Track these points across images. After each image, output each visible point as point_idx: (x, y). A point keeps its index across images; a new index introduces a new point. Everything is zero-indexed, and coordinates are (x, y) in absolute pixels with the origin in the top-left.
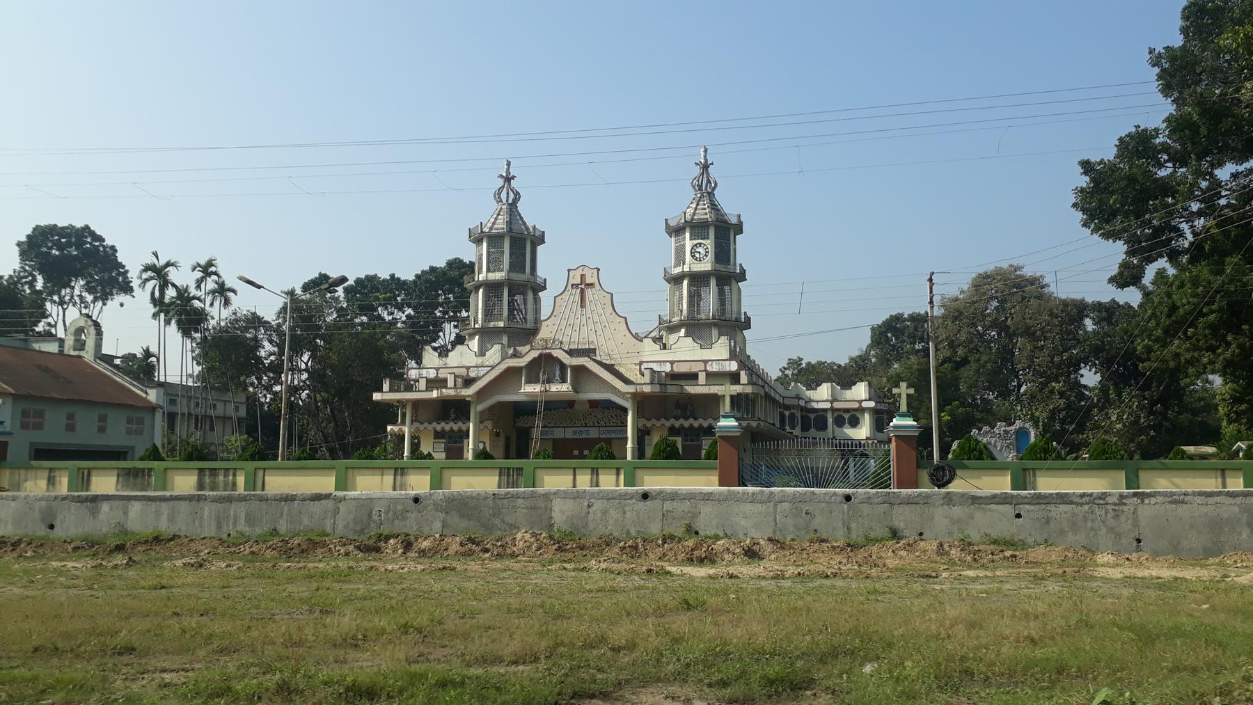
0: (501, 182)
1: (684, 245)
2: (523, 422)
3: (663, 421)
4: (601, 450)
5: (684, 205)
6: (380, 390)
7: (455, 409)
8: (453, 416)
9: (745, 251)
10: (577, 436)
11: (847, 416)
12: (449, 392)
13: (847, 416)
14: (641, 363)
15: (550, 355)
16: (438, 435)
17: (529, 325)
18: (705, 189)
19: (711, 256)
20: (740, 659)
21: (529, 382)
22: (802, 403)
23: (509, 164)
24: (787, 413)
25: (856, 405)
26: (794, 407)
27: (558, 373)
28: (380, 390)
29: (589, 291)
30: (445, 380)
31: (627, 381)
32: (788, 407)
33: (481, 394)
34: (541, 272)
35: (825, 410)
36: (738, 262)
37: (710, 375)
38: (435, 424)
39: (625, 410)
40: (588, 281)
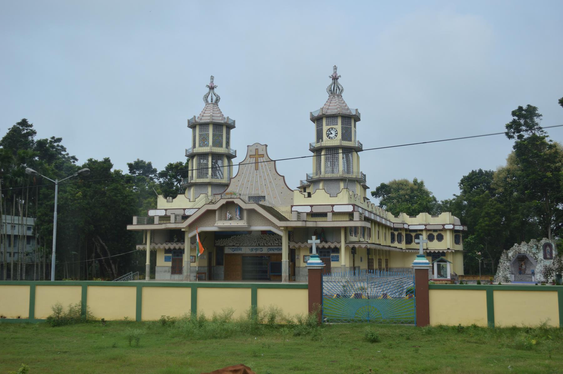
1: (322, 130)
2: (220, 243)
4: (356, 233)
6: (131, 223)
7: (176, 235)
8: (176, 239)
9: (362, 133)
10: (254, 252)
11: (435, 234)
12: (171, 225)
13: (435, 234)
14: (292, 206)
15: (233, 203)
16: (167, 251)
17: (225, 181)
18: (335, 90)
19: (340, 136)
21: (220, 219)
22: (406, 226)
23: (212, 78)
24: (396, 233)
25: (441, 227)
26: (401, 229)
27: (238, 213)
28: (131, 223)
30: (169, 217)
31: (281, 218)
32: (396, 229)
33: (192, 226)
34: (233, 146)
35: (422, 230)
36: (357, 140)
37: (334, 214)
38: (164, 245)
39: (280, 238)
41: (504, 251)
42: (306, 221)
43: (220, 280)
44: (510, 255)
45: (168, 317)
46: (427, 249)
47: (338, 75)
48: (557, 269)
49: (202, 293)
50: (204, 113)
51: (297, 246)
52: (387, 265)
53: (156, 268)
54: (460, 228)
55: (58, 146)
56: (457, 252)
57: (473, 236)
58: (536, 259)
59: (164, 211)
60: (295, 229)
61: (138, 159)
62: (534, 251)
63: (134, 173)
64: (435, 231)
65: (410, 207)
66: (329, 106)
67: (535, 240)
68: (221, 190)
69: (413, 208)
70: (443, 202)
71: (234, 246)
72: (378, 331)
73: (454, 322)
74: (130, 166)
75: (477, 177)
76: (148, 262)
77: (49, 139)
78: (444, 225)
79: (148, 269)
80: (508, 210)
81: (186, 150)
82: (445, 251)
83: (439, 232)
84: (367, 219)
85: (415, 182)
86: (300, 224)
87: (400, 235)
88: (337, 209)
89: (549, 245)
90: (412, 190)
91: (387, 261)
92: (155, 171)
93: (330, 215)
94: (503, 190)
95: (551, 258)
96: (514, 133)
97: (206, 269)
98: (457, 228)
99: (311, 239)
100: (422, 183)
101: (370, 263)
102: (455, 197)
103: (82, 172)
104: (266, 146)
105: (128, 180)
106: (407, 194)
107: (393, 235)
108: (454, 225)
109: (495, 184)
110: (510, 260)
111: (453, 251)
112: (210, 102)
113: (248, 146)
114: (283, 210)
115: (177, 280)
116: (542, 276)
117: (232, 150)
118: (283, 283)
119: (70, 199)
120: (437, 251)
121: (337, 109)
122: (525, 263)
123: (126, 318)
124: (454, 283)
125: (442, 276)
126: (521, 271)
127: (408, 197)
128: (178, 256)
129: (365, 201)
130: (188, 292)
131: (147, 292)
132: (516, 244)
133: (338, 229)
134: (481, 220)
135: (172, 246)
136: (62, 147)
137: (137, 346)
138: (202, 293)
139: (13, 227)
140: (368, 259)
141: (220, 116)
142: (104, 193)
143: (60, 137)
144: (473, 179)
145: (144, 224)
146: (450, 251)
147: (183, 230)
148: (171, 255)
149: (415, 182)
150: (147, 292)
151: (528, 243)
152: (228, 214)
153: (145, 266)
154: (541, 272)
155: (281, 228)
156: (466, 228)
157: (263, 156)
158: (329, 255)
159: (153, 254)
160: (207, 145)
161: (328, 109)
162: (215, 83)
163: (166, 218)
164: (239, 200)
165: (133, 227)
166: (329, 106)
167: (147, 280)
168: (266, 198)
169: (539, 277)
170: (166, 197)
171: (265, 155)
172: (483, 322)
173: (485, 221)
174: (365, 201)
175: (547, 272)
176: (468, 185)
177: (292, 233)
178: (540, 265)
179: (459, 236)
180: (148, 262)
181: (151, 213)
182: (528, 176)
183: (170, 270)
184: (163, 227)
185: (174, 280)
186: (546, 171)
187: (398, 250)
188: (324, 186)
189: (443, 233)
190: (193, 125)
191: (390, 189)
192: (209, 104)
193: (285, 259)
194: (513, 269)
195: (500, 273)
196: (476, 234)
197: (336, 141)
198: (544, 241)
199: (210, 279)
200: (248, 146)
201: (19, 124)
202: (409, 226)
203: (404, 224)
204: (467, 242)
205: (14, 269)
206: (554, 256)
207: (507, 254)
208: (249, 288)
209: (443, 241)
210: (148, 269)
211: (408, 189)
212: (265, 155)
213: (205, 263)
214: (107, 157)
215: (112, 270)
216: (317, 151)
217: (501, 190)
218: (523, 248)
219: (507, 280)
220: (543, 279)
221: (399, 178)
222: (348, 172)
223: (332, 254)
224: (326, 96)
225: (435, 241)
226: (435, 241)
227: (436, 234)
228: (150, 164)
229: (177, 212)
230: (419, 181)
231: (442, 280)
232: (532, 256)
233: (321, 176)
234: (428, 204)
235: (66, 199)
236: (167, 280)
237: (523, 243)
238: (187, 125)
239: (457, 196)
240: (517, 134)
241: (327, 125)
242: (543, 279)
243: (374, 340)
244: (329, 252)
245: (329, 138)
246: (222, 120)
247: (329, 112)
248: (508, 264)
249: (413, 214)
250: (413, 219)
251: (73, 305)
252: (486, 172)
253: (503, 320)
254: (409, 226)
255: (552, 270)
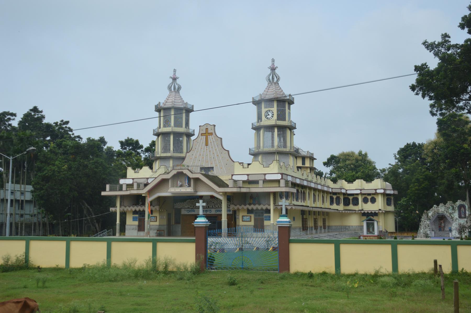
0: (171, 80)
1: (261, 111)
2: (178, 206)
3: (243, 206)
5: (260, 88)
6: (105, 190)
7: (139, 200)
8: (141, 203)
9: (295, 114)
12: (135, 192)
13: (369, 197)
14: (232, 175)
15: (182, 173)
16: (135, 212)
17: (183, 155)
18: (273, 78)
19: (275, 117)
20: (413, 279)
21: (173, 186)
22: (343, 191)
23: (175, 71)
24: (335, 197)
25: (374, 192)
26: (339, 193)
27: (187, 182)
28: (105, 190)
29: (210, 138)
32: (335, 194)
33: (151, 192)
35: (358, 194)
37: (265, 181)
38: (131, 207)
39: (220, 201)
40: (209, 132)
41: (425, 211)
42: (240, 187)
43: (178, 236)
44: (430, 214)
45: (88, 265)
46: (362, 210)
47: (275, 66)
48: (469, 227)
49: (160, 246)
50: (168, 100)
51: (236, 208)
52: (324, 223)
53: (126, 227)
54: (392, 192)
55: (66, 127)
56: (387, 213)
57: (406, 199)
58: (452, 218)
59: (131, 180)
60: (234, 194)
61: (128, 138)
62: (450, 211)
63: (125, 149)
64: (369, 194)
65: (354, 175)
66: (267, 92)
67: (451, 202)
68: (178, 162)
69: (357, 175)
70: (381, 170)
71: (188, 208)
72: (237, 276)
73: (307, 270)
74: (121, 143)
75: (411, 149)
76: (118, 222)
77: (59, 122)
78: (376, 190)
79: (118, 227)
80: (436, 176)
81: (154, 130)
82: (377, 212)
83: (372, 196)
84: (294, 185)
85: (360, 153)
86: (235, 190)
87: (338, 199)
88: (268, 177)
89: (464, 207)
90: (357, 160)
91: (324, 221)
92: (142, 147)
93: (261, 182)
94: (432, 160)
95: (465, 217)
96: (437, 111)
97: (166, 227)
98: (388, 192)
99: (199, 203)
100: (366, 154)
101: (304, 221)
102: (390, 166)
103: (29, 150)
104: (215, 126)
105: (119, 154)
106: (352, 164)
107: (332, 199)
108: (384, 189)
109: (425, 154)
110: (430, 219)
111: (384, 212)
112: (173, 90)
113: (200, 126)
114: (225, 178)
115: (142, 236)
116: (457, 232)
117: (192, 130)
118: (418, 239)
119: (57, 171)
120: (370, 212)
121: (273, 94)
122: (444, 222)
123: (57, 266)
124: (381, 238)
125: (371, 233)
126: (441, 229)
127: (354, 166)
128: (259, 216)
129: (298, 170)
130: (150, 245)
131: (115, 245)
132: (435, 206)
133: (268, 194)
134: (412, 185)
135: (138, 208)
136: (69, 128)
137: (44, 287)
138: (160, 246)
139: (22, 193)
140: (303, 218)
141: (181, 102)
142: (86, 166)
143: (67, 120)
144: (407, 151)
145: (116, 191)
146: (380, 212)
147: (143, 195)
148: (137, 216)
149: (360, 153)
150: (115, 245)
151: (445, 204)
152: (179, 182)
153: (116, 224)
154: (456, 229)
155: (220, 194)
156: (396, 192)
157: (211, 134)
158: (263, 216)
159: (123, 215)
160: (169, 126)
161: (266, 94)
162: (177, 75)
163: (130, 186)
164: (187, 170)
165: (107, 193)
166: (267, 92)
167: (117, 236)
168: (214, 168)
169: (455, 233)
170: (134, 169)
171: (214, 133)
172: (332, 269)
173: (415, 186)
174: (298, 170)
175: (461, 229)
176: (402, 156)
177: (230, 198)
178: (456, 222)
179: (391, 199)
180: (118, 222)
181: (122, 181)
182: (448, 147)
183: (137, 228)
184: (128, 193)
185: (140, 236)
186: (463, 143)
187: (333, 211)
188: (262, 159)
189: (375, 197)
190: (158, 109)
191: (339, 160)
192: (172, 92)
193: (224, 219)
194: (433, 227)
195: (422, 230)
196: (408, 197)
197: (273, 121)
198: (459, 203)
199: (169, 235)
200: (200, 126)
201: (31, 110)
202: (347, 190)
203: (341, 189)
204: (400, 204)
205: (229, 226)
206: (467, 215)
207: (428, 214)
208: (193, 242)
209: (376, 203)
210: (118, 227)
211: (353, 160)
212: (214, 133)
213: (165, 222)
214: (102, 136)
215: (96, 228)
216: (257, 129)
217: (429, 159)
218: (441, 209)
219: (427, 236)
220: (458, 235)
221: (347, 150)
222: (285, 146)
223: (265, 215)
224: (266, 84)
225: (369, 203)
226: (369, 203)
227: (370, 197)
228: (137, 142)
229: (139, 181)
230: (363, 153)
231: (370, 236)
232: (449, 215)
233: (260, 150)
234: (370, 172)
235: (54, 171)
236: (134, 236)
237: (441, 205)
238: (154, 109)
239: (392, 165)
240: (439, 112)
241: (265, 108)
242: (458, 235)
243: (232, 283)
244: (262, 213)
245: (267, 119)
246: (182, 105)
247: (267, 97)
248: (428, 223)
249: (350, 181)
250: (351, 185)
251: (19, 256)
252: (419, 144)
253: (347, 268)
254: (347, 190)
255: (466, 227)
